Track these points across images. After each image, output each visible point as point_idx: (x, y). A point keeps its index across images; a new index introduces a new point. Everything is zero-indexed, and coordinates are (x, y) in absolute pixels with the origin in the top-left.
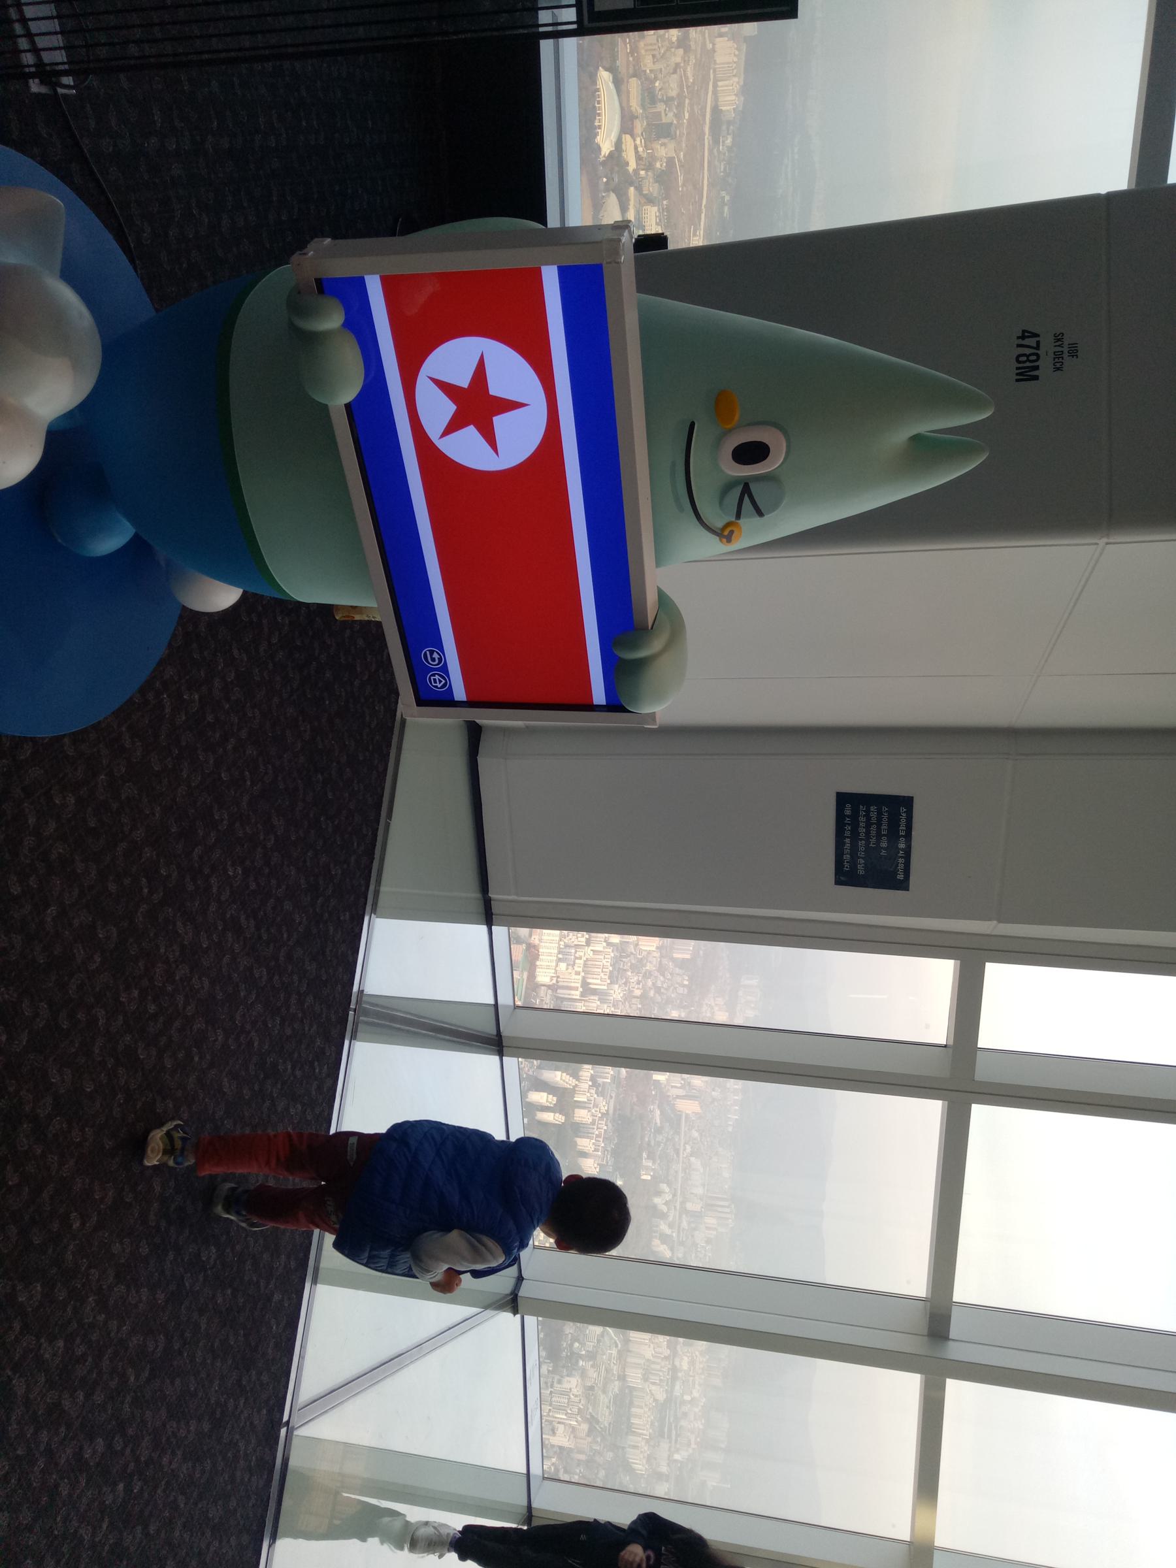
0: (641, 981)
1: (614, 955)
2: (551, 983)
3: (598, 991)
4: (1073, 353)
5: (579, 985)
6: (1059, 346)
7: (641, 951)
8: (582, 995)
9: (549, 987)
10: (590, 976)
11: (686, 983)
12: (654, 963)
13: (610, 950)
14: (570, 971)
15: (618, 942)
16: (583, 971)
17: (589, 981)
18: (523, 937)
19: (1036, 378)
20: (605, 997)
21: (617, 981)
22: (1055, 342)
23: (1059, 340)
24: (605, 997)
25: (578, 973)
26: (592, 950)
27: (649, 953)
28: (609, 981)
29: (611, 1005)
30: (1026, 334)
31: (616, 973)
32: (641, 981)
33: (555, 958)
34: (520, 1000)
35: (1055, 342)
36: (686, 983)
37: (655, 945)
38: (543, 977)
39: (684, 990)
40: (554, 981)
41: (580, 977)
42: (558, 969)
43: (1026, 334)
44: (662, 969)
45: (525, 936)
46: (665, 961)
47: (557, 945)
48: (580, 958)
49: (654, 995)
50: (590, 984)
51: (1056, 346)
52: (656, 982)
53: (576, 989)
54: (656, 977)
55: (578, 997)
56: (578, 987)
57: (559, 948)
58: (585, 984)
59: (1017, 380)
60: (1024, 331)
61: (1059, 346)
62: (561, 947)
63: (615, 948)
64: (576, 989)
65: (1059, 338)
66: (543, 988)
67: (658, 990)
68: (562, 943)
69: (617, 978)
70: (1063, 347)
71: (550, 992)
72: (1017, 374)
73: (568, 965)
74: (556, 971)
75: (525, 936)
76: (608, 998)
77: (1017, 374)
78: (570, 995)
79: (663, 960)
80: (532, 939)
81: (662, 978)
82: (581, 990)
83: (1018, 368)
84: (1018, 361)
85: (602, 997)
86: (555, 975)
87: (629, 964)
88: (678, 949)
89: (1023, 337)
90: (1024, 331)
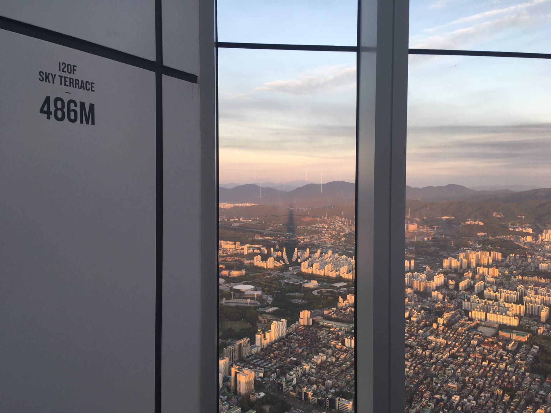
0: (514, 276)
1: (502, 288)
2: (518, 319)
3: (520, 295)
4: (62, 109)
5: (518, 306)
6: (53, 79)
7: (499, 276)
8: (523, 304)
9: (520, 320)
10: (513, 301)
11: (514, 255)
12: (505, 269)
13: (500, 290)
14: (511, 310)
15: (495, 286)
16: (511, 303)
17: (515, 301)
18: (496, 332)
19: (92, 106)
20: (523, 293)
21: (515, 287)
22: (49, 82)
23: (47, 77)
24: (523, 293)
25: (512, 306)
26: (500, 299)
27: (500, 272)
28: (515, 291)
29: (527, 290)
30: (45, 109)
31: (511, 288)
32: (514, 276)
33: (505, 316)
34: (527, 334)
35: (49, 82)
36: (514, 255)
37: (496, 269)
38: (515, 322)
39: (534, 348)
40: (517, 317)
41: (514, 305)
42: (510, 316)
43: (45, 109)
44: (507, 266)
45: (495, 331)
46: (504, 264)
47: (499, 315)
48: (504, 305)
49: (521, 270)
50: (517, 300)
51: (53, 83)
52: (514, 269)
53: (520, 307)
54: (512, 269)
55: (524, 306)
56: (519, 306)
57: (500, 314)
58: (517, 303)
59: (93, 123)
60: (42, 111)
61: (53, 79)
62: (499, 313)
63: (498, 288)
64: (520, 307)
65: (45, 77)
66: (521, 323)
67: (518, 268)
68: (497, 313)
69: (513, 287)
70: (55, 75)
71: (522, 319)
72: (87, 123)
73: (508, 310)
74: (511, 316)
75: (495, 331)
76: (524, 292)
77: (87, 123)
78: (523, 312)
79: (503, 266)
80: (496, 327)
81: (512, 266)
82: (520, 305)
83: (82, 122)
84: (74, 121)
85: (524, 295)
86: (514, 317)
87: (506, 281)
88: (498, 256)
89: (48, 113)
90: (42, 111)
